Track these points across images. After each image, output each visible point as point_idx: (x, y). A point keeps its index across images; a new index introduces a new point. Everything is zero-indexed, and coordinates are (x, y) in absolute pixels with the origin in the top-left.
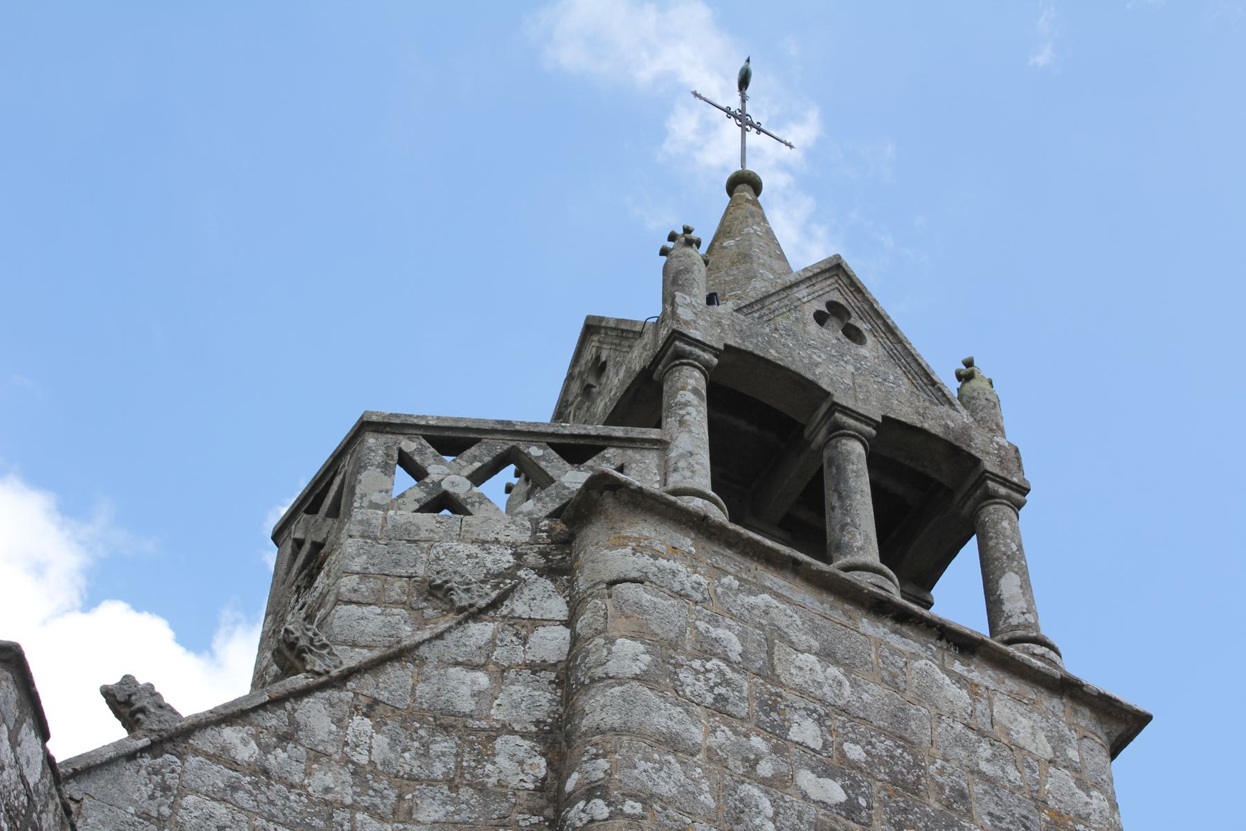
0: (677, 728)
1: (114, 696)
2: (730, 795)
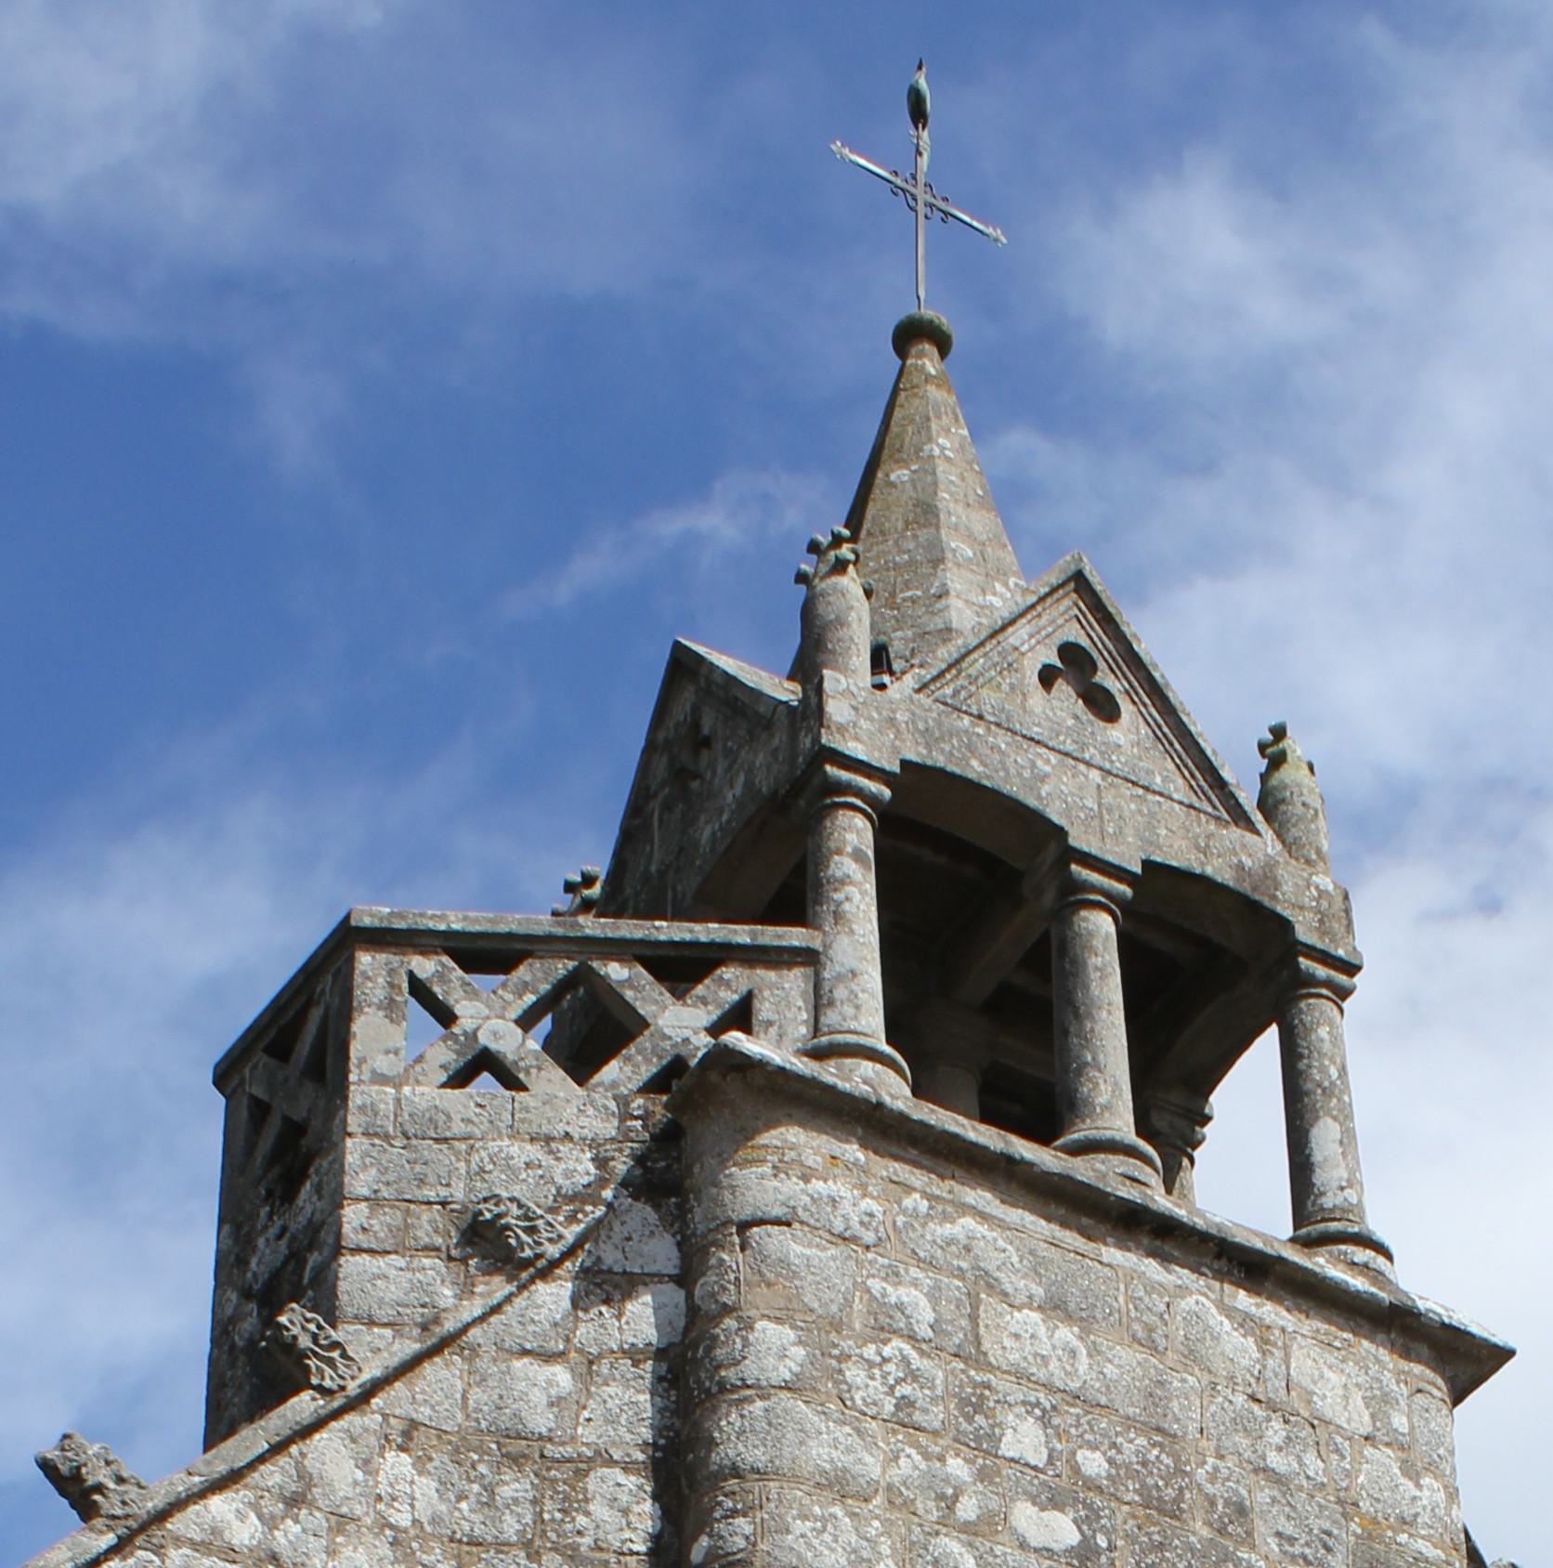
1: (56, 1468)
2: (919, 1556)
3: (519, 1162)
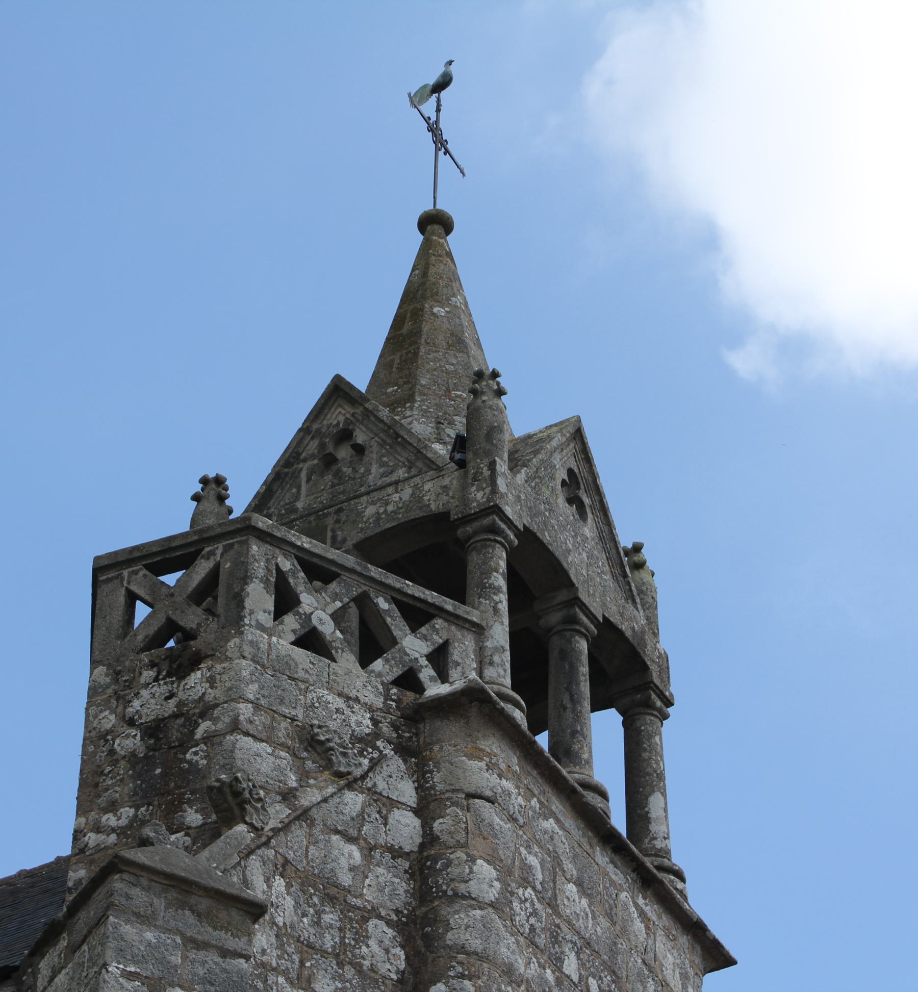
3: (332, 707)
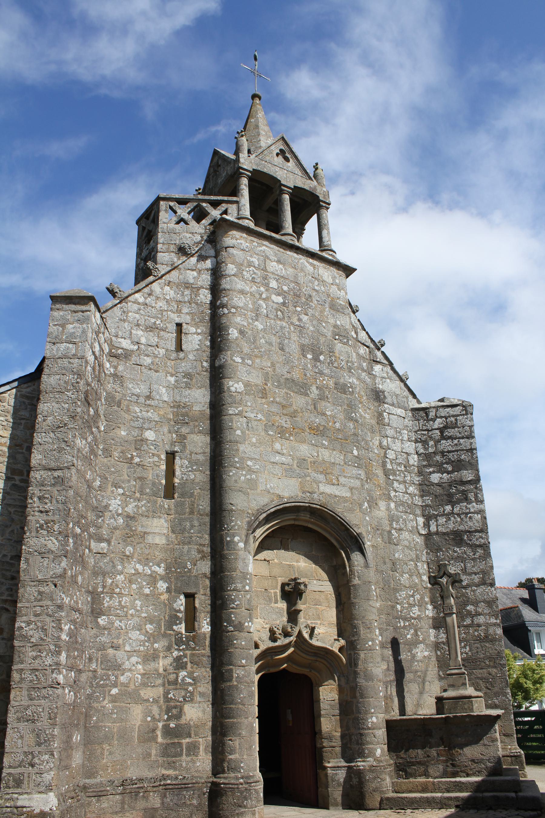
0: (243, 288)
3: (188, 237)
